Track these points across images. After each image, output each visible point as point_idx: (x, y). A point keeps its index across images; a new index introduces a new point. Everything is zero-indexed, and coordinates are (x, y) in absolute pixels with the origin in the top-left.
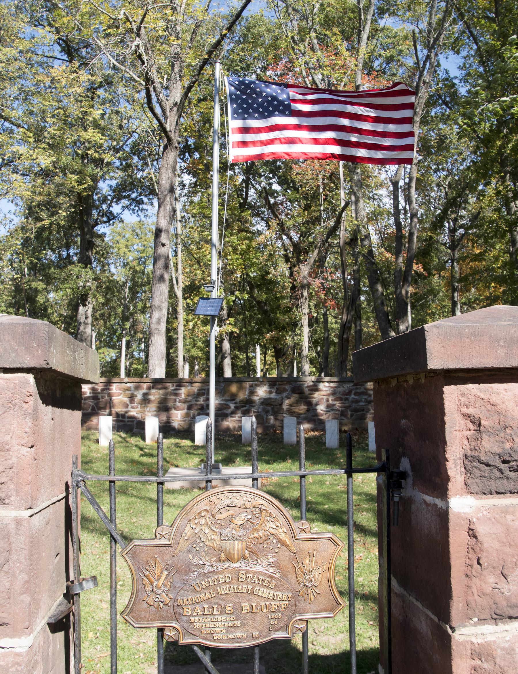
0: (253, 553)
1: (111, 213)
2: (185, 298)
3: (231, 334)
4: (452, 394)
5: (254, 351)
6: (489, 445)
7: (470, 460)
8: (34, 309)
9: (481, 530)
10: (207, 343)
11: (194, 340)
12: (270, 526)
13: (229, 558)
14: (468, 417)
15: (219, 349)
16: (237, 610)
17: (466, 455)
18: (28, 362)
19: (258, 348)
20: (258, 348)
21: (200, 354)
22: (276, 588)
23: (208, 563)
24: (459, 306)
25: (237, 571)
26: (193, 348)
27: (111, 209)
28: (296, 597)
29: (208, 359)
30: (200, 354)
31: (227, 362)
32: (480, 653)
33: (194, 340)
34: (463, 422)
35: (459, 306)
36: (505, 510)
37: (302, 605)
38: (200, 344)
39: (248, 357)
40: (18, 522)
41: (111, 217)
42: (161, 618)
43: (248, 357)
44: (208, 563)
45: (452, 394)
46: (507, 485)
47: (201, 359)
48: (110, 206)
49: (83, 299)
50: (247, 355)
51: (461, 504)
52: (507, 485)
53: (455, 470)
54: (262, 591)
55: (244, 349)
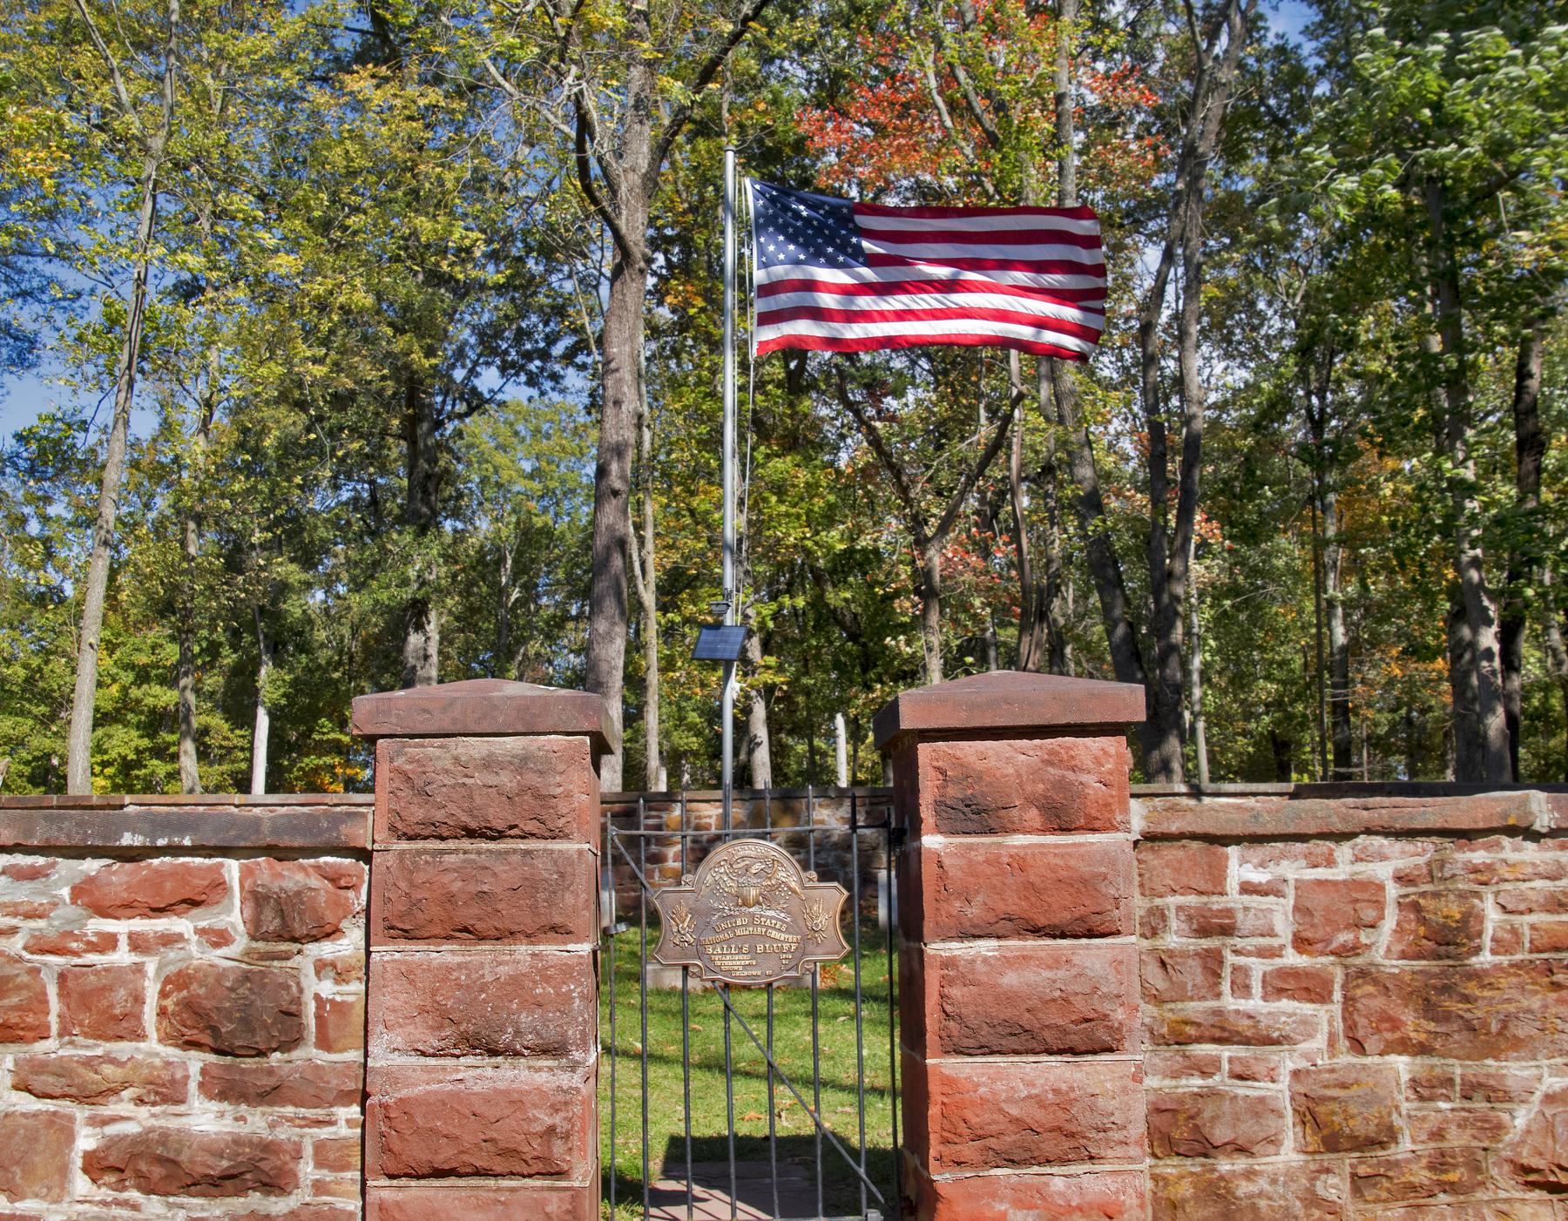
0: (766, 899)
1: (474, 390)
2: (663, 608)
3: (769, 691)
4: (925, 750)
5: (831, 735)
6: (952, 791)
7: (940, 805)
8: (278, 634)
9: (947, 862)
10: (715, 715)
11: (680, 709)
12: (782, 875)
13: (745, 904)
14: (937, 769)
15: (741, 728)
16: (752, 951)
17: (1227, 931)
18: (586, 727)
19: (840, 720)
20: (840, 720)
21: (694, 742)
22: (787, 931)
23: (726, 906)
24: (1340, 611)
25: (753, 915)
26: (676, 727)
27: (476, 382)
28: (805, 940)
29: (717, 754)
30: (694, 742)
31: (762, 757)
32: (949, 963)
33: (680, 709)
34: (932, 774)
35: (1340, 611)
36: (970, 847)
37: (810, 948)
38: (694, 717)
39: (813, 750)
40: (580, 852)
41: (476, 403)
42: (686, 957)
43: (813, 750)
44: (726, 906)
45: (925, 750)
46: (971, 826)
47: (695, 754)
48: (473, 372)
49: (416, 612)
50: (811, 744)
51: (931, 841)
52: (971, 826)
53: (927, 813)
54: (774, 934)
55: (804, 729)
